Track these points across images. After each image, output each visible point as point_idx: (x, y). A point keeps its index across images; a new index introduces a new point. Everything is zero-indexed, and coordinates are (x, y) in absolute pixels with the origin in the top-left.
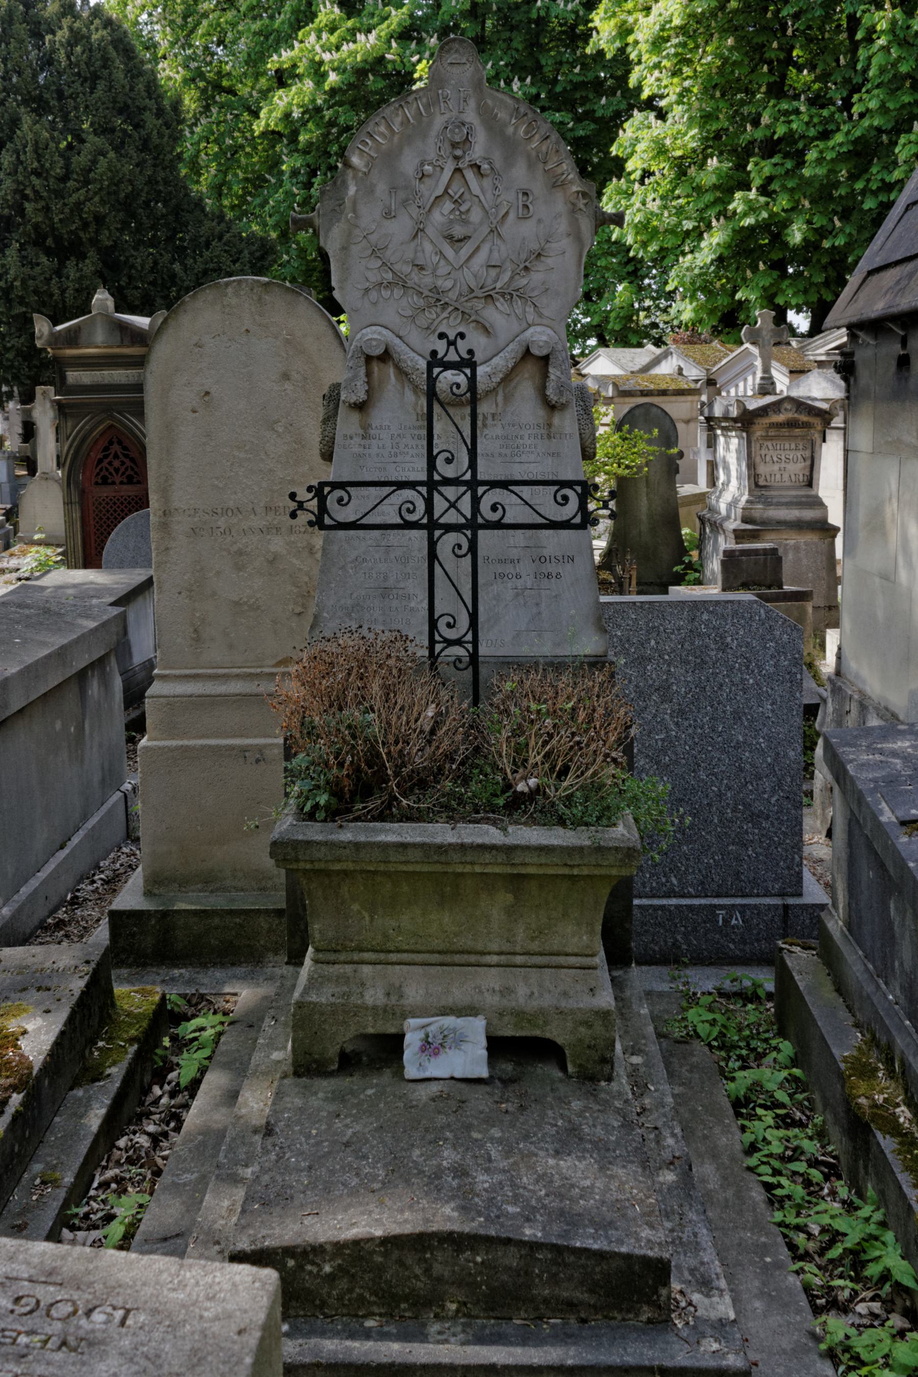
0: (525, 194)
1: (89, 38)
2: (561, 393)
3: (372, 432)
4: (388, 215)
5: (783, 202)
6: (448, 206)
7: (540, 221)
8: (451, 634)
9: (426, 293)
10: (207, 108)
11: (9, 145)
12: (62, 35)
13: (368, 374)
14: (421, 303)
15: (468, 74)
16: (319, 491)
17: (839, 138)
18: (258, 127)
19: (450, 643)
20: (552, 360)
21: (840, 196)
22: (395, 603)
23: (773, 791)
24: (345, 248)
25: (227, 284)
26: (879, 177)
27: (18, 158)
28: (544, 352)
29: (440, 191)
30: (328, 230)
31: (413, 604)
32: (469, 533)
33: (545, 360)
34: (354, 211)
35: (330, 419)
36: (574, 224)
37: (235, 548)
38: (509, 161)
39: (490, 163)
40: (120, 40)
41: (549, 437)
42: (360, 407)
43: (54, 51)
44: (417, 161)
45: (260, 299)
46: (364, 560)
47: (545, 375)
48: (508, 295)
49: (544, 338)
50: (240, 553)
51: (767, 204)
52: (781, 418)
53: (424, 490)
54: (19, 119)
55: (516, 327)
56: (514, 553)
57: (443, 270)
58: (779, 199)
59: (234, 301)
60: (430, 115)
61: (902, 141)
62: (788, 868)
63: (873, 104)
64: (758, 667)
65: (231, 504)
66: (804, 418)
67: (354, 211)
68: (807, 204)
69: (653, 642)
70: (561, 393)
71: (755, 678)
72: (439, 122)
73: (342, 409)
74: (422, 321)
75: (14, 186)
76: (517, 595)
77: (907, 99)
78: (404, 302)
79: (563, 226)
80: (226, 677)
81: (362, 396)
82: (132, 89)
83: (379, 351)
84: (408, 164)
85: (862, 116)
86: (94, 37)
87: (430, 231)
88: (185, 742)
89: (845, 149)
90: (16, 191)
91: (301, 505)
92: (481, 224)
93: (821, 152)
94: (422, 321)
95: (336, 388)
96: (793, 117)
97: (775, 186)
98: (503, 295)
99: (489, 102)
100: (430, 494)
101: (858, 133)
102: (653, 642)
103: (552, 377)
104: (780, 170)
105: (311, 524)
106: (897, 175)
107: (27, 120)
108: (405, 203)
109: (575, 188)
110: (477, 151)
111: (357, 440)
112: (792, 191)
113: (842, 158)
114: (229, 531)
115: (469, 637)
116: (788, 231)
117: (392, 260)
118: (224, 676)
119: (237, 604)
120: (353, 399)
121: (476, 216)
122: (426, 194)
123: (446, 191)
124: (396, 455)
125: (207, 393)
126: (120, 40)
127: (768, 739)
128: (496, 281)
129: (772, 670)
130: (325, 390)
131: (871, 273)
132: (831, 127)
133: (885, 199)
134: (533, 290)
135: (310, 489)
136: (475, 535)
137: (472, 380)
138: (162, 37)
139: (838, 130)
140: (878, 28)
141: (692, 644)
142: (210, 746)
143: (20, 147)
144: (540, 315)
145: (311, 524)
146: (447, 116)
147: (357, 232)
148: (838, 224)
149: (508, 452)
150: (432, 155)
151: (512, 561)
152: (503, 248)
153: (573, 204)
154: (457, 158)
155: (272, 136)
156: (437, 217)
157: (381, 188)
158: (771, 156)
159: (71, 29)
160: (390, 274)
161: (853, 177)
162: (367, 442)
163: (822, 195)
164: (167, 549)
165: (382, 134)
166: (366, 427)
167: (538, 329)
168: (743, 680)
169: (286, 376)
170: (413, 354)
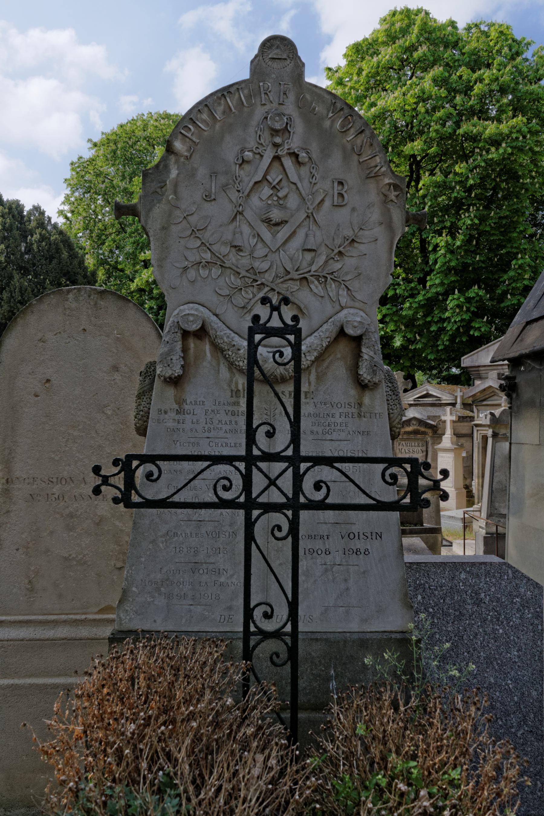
0: (341, 183)
1: (50, 239)
2: (374, 372)
3: (186, 407)
4: (208, 198)
5: (391, 327)
6: (266, 191)
7: (354, 209)
8: (269, 626)
9: (243, 273)
10: (109, 278)
11: (7, 288)
12: (36, 237)
13: (185, 350)
14: (239, 282)
15: (288, 69)
16: (126, 465)
17: (420, 298)
18: (133, 286)
19: (266, 635)
20: (364, 341)
21: (419, 325)
22: (205, 578)
23: (519, 726)
24: (164, 228)
25: (69, 291)
26: (439, 315)
27: (11, 295)
28: (359, 332)
29: (258, 177)
30: (149, 210)
31: (222, 579)
32: (289, 513)
33: (358, 340)
34: (175, 193)
35: (145, 393)
36: (386, 213)
37: (67, 511)
38: (325, 153)
39: (308, 153)
40: (67, 241)
41: (359, 416)
42: (175, 382)
43: (32, 244)
44: (238, 148)
45: (96, 304)
46: (176, 534)
47: (358, 355)
48: (323, 278)
49: (359, 319)
50: (71, 516)
51: (383, 328)
52: (410, 429)
53: (242, 466)
54: (13, 277)
55: (329, 309)
56: (323, 530)
57: (260, 251)
58: (390, 325)
59: (74, 305)
60: (251, 105)
61: (450, 298)
62: (532, 793)
63: (437, 281)
64: (507, 619)
65: (65, 474)
66: (422, 429)
67: (175, 193)
68: (403, 328)
69: (420, 597)
70: (374, 372)
71: (504, 629)
72: (259, 113)
73: (157, 384)
74: (239, 300)
75: (9, 308)
76: (326, 570)
77: (453, 279)
78: (221, 282)
79: (375, 215)
80: (55, 623)
81: (178, 371)
82: (71, 264)
83: (195, 327)
84: (229, 151)
85: (431, 286)
86: (52, 238)
87: (248, 214)
88: (16, 681)
89: (422, 303)
90: (9, 311)
91: (106, 480)
92: (298, 209)
93: (411, 303)
94: (239, 300)
95: (152, 365)
96: (396, 287)
97: (387, 319)
98: (317, 277)
99: (308, 96)
100: (248, 469)
101: (429, 295)
102: (420, 597)
103: (365, 357)
104: (391, 312)
105: (116, 500)
106: (447, 314)
107: (16, 277)
108: (224, 188)
109: (387, 181)
110: (295, 142)
111: (172, 415)
112: (396, 322)
113: (421, 306)
114: (61, 497)
115: (288, 628)
116: (394, 341)
117: (211, 240)
118: (53, 621)
119: (66, 559)
120: (168, 373)
121: (293, 202)
122: (246, 179)
123: (265, 178)
124: (209, 431)
125: (48, 381)
126: (67, 241)
127: (515, 680)
128: (311, 264)
129: (518, 621)
130: (143, 368)
131: (528, 323)
132: (416, 292)
133: (441, 326)
134: (347, 273)
135: (116, 462)
136: (296, 516)
137: (296, 348)
138: (86, 243)
139: (419, 293)
140: (440, 245)
141: (452, 599)
142: (37, 685)
143: (12, 289)
144: (353, 298)
145: (116, 500)
146: (267, 108)
147: (178, 213)
148: (418, 338)
149: (320, 429)
150: (252, 144)
151: (322, 537)
152: (318, 233)
153: (385, 196)
154: (276, 146)
155: (141, 291)
156: (255, 201)
157: (202, 172)
158: (386, 305)
159: (40, 234)
160: (209, 254)
161: (425, 316)
162: (181, 417)
163: (410, 323)
164: (8, 512)
165: (204, 121)
166: (180, 402)
167: (352, 311)
168: (494, 630)
169: (115, 368)
170: (228, 331)
